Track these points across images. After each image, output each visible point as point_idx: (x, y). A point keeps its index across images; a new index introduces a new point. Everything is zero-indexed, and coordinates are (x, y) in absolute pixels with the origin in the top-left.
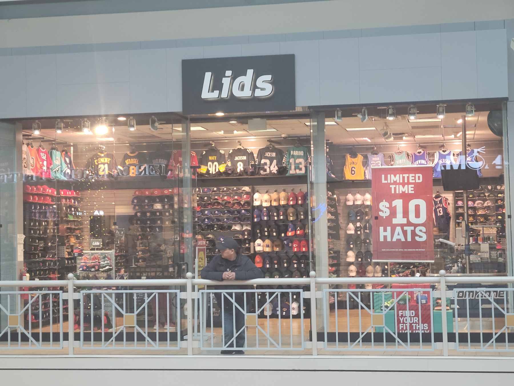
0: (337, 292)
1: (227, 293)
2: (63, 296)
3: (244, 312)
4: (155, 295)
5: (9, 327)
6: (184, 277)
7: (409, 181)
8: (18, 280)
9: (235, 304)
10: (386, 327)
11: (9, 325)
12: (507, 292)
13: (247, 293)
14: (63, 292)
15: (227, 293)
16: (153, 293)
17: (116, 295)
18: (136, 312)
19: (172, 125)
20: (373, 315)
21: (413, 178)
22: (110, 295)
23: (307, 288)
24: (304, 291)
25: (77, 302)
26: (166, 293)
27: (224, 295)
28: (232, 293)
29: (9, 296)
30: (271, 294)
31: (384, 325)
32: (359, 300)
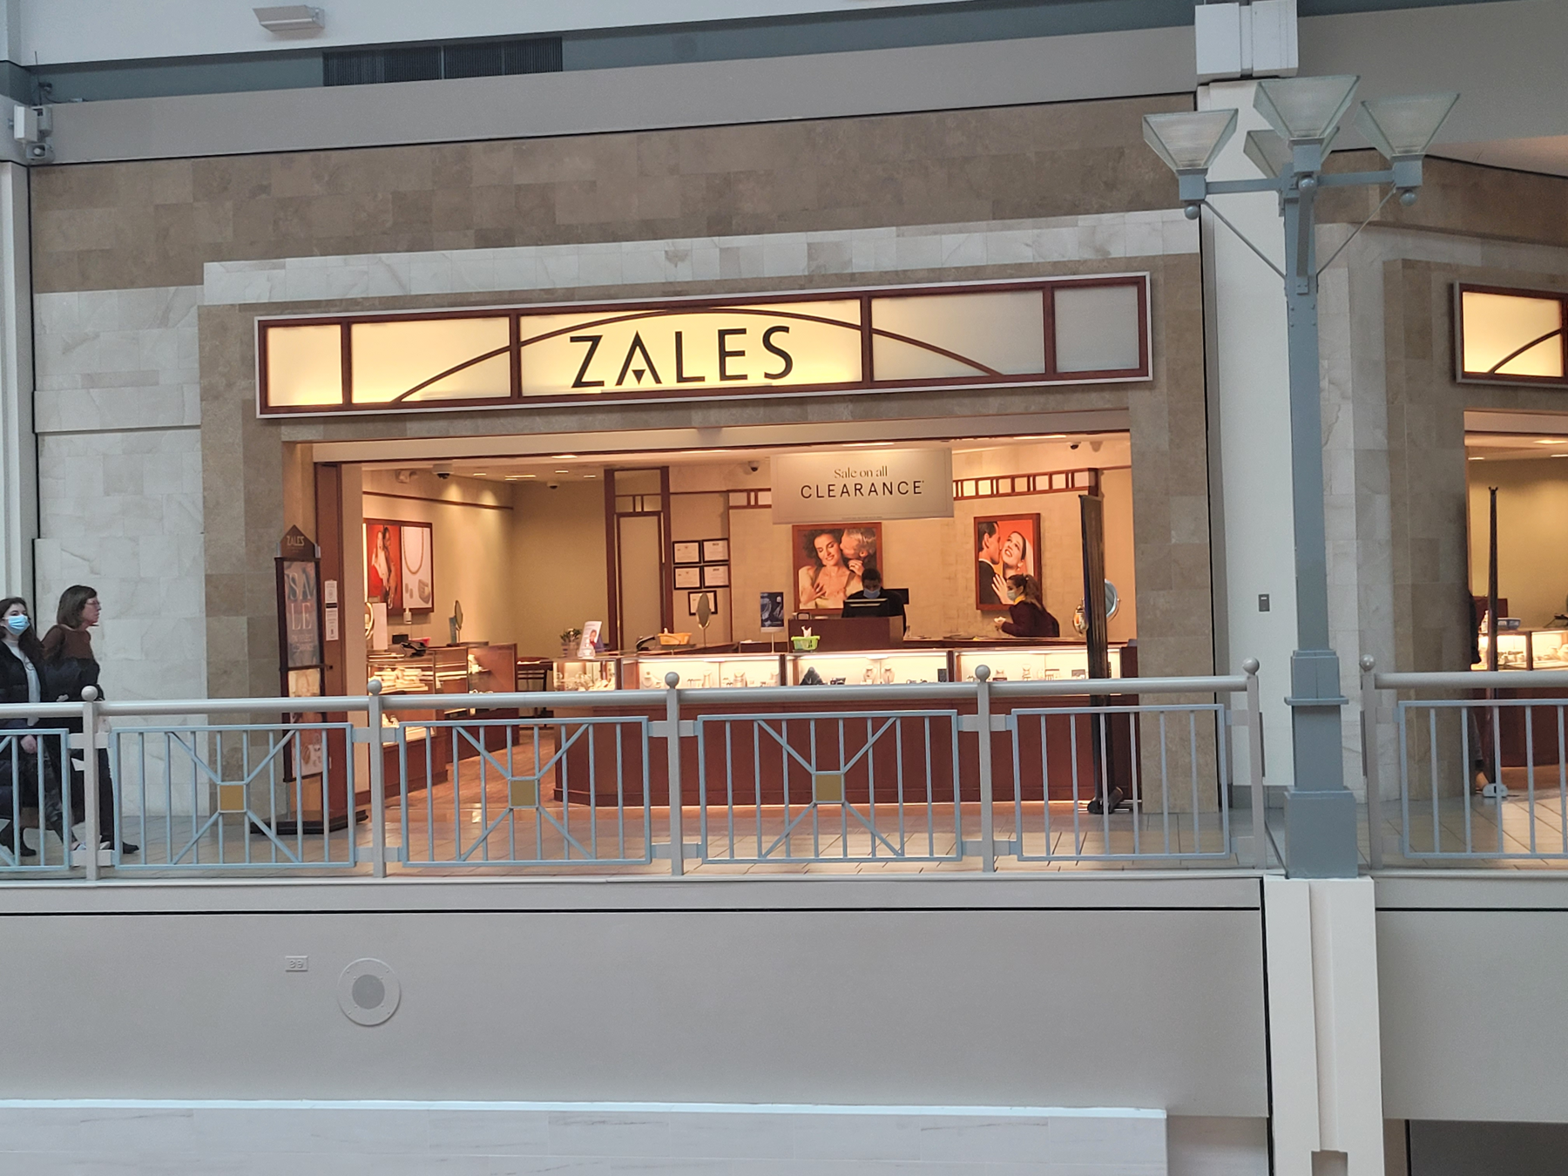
0: (1135, 713)
1: (766, 721)
2: (71, 741)
3: (812, 769)
4: (10, 743)
5: (221, 814)
6: (76, 697)
7: (728, 356)
8: (37, 702)
9: (787, 748)
10: (250, 814)
11: (221, 809)
12: (1137, 714)
13: (1501, 708)
14: (71, 732)
15: (768, 721)
16: (889, 718)
17: (44, 739)
18: (844, 769)
19: (37, 61)
20: (817, 776)
21: (732, 343)
22: (473, 731)
23: (75, 724)
24: (650, 720)
25: (687, 744)
26: (505, 727)
27: (459, 733)
28: (477, 728)
29: (1433, 713)
30: (878, 722)
31: (245, 810)
32: (783, 741)
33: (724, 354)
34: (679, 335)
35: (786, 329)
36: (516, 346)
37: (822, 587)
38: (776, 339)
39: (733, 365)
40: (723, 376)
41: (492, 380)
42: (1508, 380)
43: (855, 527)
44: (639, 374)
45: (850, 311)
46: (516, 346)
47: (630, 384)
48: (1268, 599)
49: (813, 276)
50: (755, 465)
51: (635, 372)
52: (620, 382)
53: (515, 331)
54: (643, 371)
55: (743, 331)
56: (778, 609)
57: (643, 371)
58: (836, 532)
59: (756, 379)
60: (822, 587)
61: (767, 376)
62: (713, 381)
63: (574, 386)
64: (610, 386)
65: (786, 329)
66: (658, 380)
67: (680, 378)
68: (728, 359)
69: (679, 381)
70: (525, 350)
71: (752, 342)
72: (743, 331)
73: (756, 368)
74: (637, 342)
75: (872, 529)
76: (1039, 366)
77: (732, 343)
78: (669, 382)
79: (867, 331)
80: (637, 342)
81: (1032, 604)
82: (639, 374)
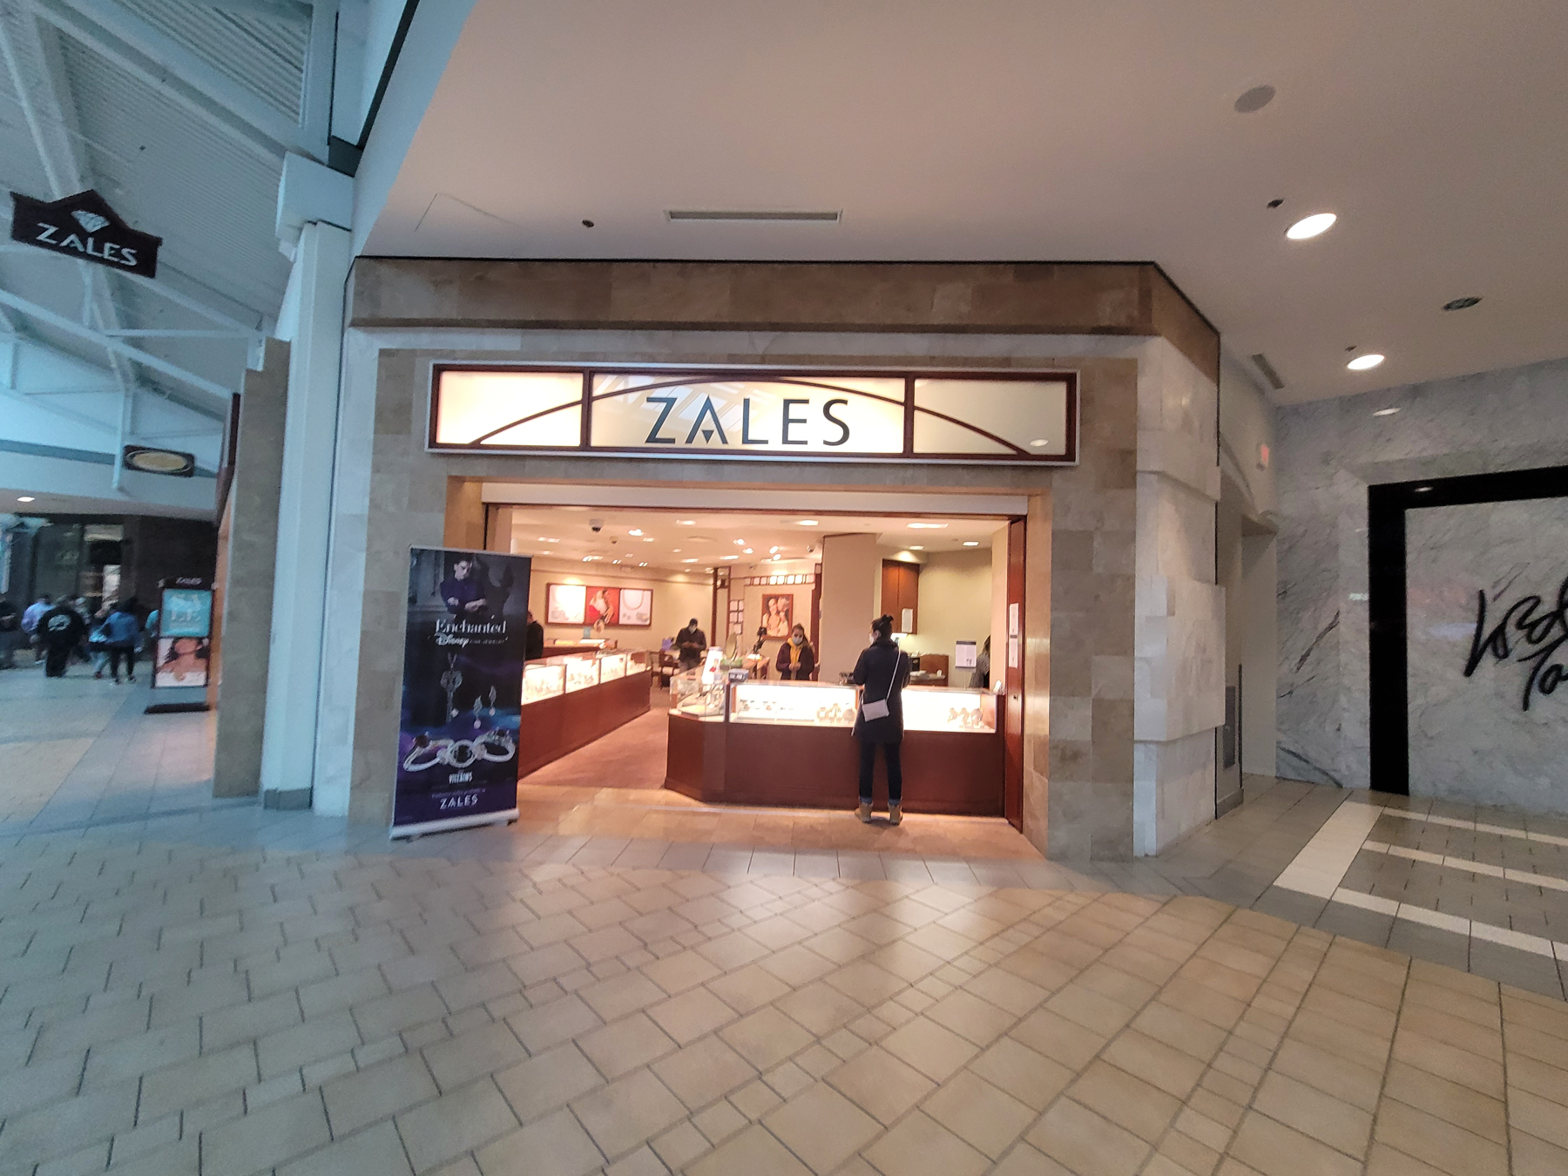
21: (795, 411)
33: (787, 421)
34: (747, 402)
35: (845, 402)
36: (587, 401)
37: (695, 680)
38: (835, 410)
39: (795, 432)
40: (785, 441)
41: (563, 432)
42: (1046, 460)
43: (783, 596)
44: (708, 434)
45: (896, 388)
46: (587, 401)
47: (699, 442)
48: (919, 662)
49: (766, 355)
50: (614, 540)
51: (704, 431)
52: (690, 440)
53: (588, 388)
54: (712, 432)
55: (806, 402)
56: (1325, 594)
57: (712, 432)
58: (776, 597)
59: (816, 446)
60: (695, 680)
61: (826, 443)
62: (776, 444)
63: (647, 441)
64: (681, 443)
65: (845, 402)
66: (724, 441)
67: (746, 440)
68: (791, 425)
69: (744, 442)
70: (595, 404)
71: (813, 412)
72: (806, 402)
73: (815, 435)
74: (708, 405)
75: (790, 597)
76: (577, 442)
77: (795, 411)
78: (736, 442)
79: (909, 407)
80: (708, 405)
81: (435, 757)
82: (708, 434)
